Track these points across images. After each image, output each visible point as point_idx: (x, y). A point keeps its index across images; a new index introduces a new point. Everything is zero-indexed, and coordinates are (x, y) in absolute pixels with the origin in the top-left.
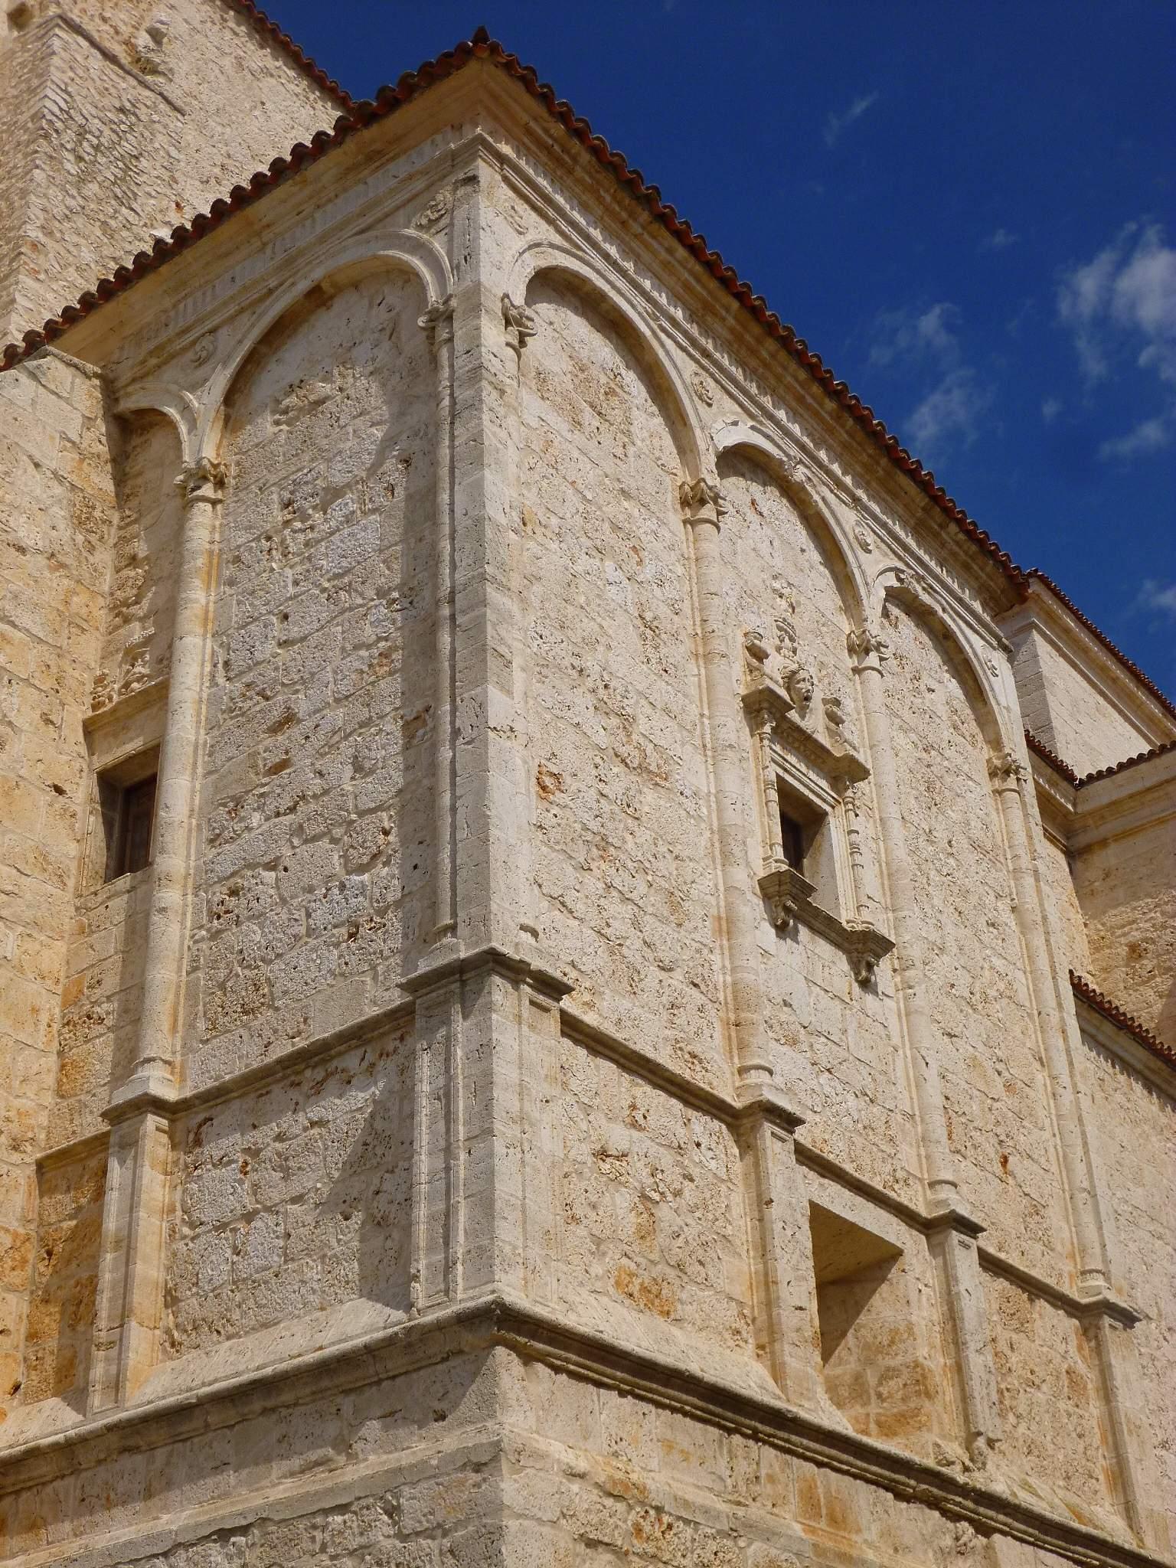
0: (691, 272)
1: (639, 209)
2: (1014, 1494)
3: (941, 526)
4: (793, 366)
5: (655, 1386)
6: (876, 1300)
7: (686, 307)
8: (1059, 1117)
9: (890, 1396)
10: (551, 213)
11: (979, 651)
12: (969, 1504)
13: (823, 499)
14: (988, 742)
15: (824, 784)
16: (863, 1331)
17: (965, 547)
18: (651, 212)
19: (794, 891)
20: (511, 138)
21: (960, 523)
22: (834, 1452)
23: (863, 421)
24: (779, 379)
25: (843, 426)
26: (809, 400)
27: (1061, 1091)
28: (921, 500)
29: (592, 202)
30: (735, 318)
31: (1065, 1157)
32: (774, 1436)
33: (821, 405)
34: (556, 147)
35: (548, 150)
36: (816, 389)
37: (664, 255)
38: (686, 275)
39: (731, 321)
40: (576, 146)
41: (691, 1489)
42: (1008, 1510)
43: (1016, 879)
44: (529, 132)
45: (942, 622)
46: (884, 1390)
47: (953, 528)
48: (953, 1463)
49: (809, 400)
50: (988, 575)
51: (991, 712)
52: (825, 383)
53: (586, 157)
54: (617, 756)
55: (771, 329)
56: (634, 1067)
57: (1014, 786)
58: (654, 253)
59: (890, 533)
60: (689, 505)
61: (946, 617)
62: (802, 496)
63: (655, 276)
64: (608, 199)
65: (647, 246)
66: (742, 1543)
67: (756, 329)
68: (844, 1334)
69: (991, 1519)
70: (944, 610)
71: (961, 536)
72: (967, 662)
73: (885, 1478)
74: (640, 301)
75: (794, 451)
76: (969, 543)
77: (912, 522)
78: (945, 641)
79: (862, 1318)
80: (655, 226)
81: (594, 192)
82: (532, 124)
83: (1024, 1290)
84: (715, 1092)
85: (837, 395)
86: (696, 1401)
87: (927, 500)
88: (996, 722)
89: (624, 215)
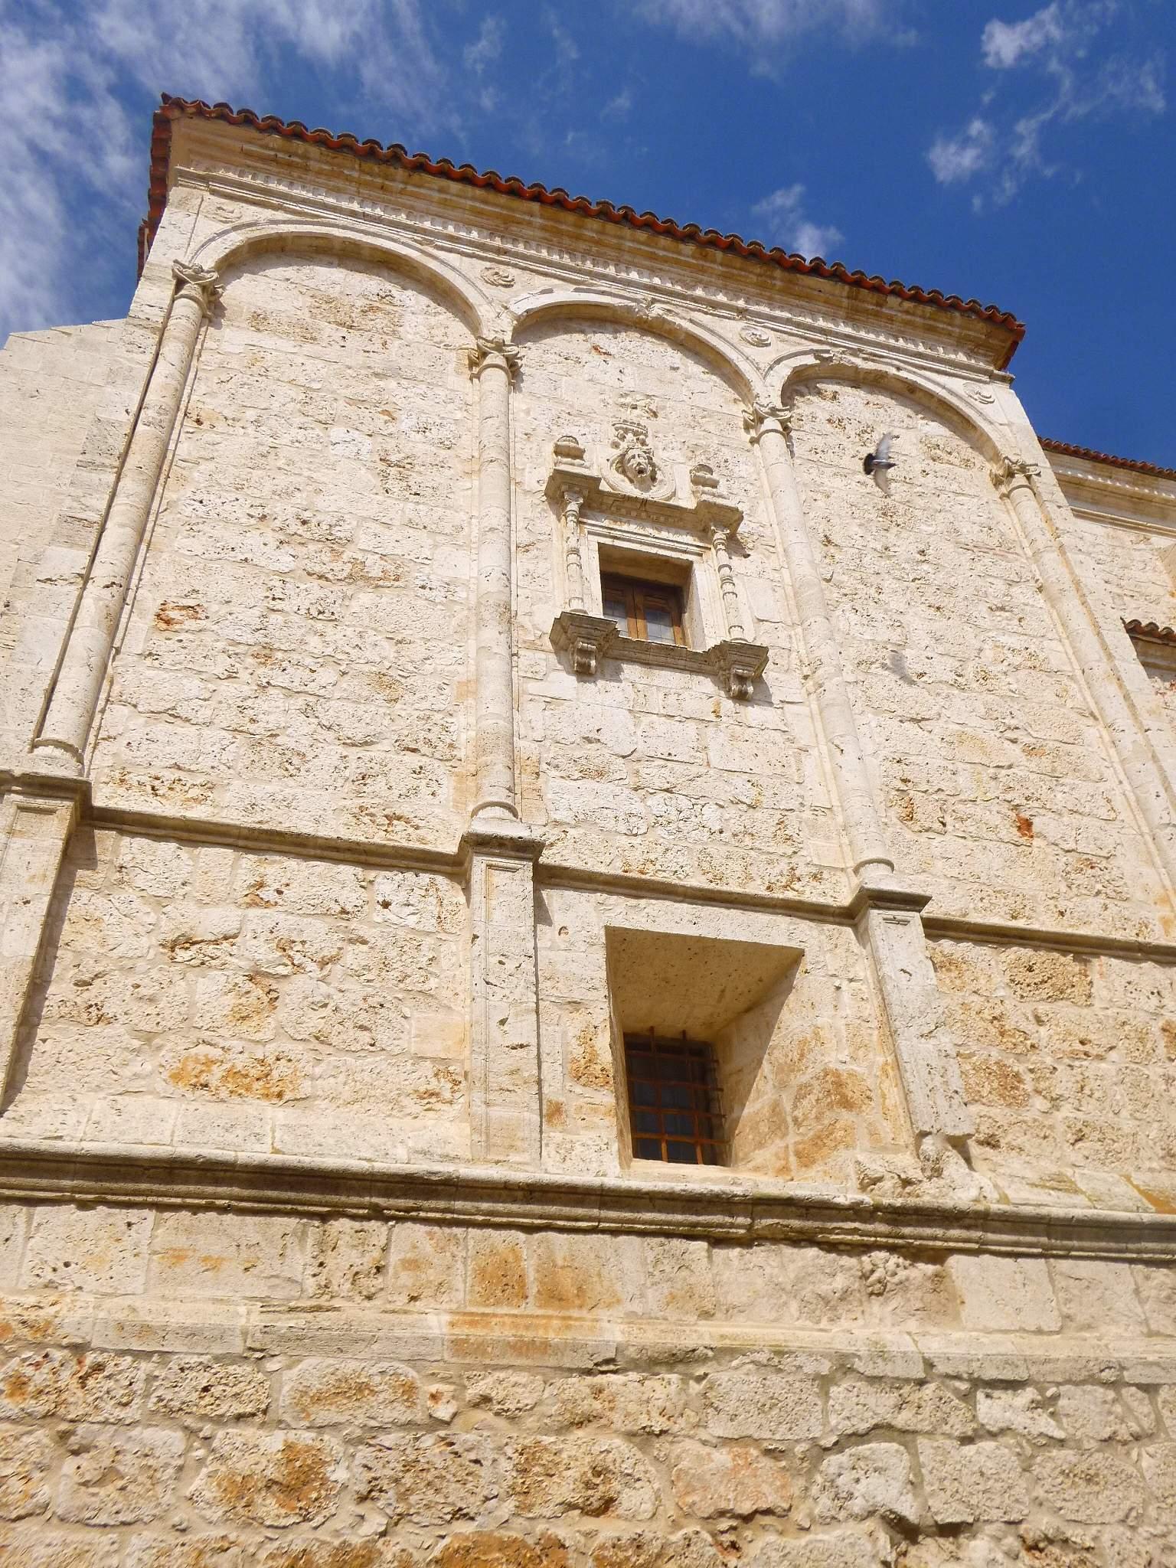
0: (473, 199)
1: (392, 170)
2: (1003, 1198)
3: (878, 304)
4: (627, 232)
5: (143, 1186)
6: (785, 1015)
7: (481, 227)
8: (1123, 761)
9: (806, 1118)
10: (274, 201)
11: (961, 392)
12: (882, 1228)
13: (691, 321)
14: (989, 460)
15: (689, 539)
16: (776, 1053)
17: (919, 312)
18: (405, 167)
19: (583, 631)
20: (229, 165)
21: (897, 292)
22: (553, 1209)
23: (731, 247)
24: (619, 248)
25: (714, 261)
26: (661, 253)
27: (1118, 735)
28: (841, 290)
29: (340, 184)
30: (542, 217)
31: (1138, 801)
32: (419, 1209)
33: (679, 253)
34: (280, 155)
35: (275, 160)
36: (664, 241)
37: (436, 195)
38: (470, 203)
39: (538, 221)
40: (299, 146)
41: (211, 1308)
42: (967, 1221)
43: (1037, 561)
44: (248, 155)
45: (904, 381)
46: (799, 1113)
47: (893, 301)
48: (880, 1179)
49: (661, 253)
50: (959, 327)
51: (983, 434)
52: (669, 231)
53: (314, 151)
54: (309, 574)
55: (582, 209)
56: (265, 846)
57: (1024, 482)
58: (424, 198)
59: (798, 325)
60: (753, 427)
61: (903, 374)
62: (667, 327)
63: (723, 289)
64: (356, 174)
65: (417, 196)
66: (271, 1365)
67: (571, 218)
68: (760, 1063)
69: (935, 1238)
70: (899, 369)
71: (907, 305)
72: (942, 402)
73: (681, 1224)
74: (406, 236)
75: (641, 294)
76: (921, 307)
77: (842, 313)
78: (911, 395)
79: (775, 1039)
80: (416, 177)
81: (339, 175)
82: (246, 147)
83: (1064, 953)
84: (428, 847)
85: (690, 236)
86: (236, 1190)
87: (847, 287)
88: (989, 439)
89: (379, 180)
